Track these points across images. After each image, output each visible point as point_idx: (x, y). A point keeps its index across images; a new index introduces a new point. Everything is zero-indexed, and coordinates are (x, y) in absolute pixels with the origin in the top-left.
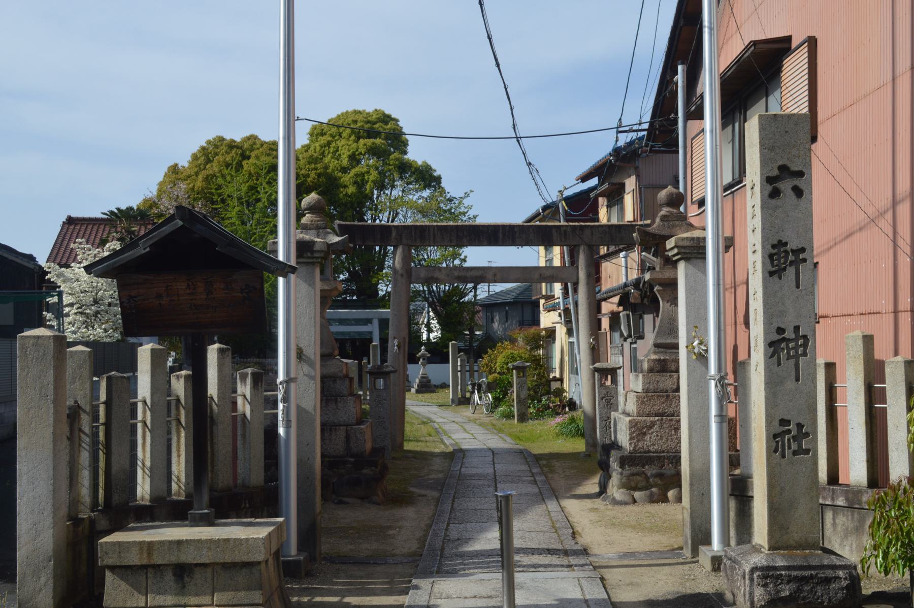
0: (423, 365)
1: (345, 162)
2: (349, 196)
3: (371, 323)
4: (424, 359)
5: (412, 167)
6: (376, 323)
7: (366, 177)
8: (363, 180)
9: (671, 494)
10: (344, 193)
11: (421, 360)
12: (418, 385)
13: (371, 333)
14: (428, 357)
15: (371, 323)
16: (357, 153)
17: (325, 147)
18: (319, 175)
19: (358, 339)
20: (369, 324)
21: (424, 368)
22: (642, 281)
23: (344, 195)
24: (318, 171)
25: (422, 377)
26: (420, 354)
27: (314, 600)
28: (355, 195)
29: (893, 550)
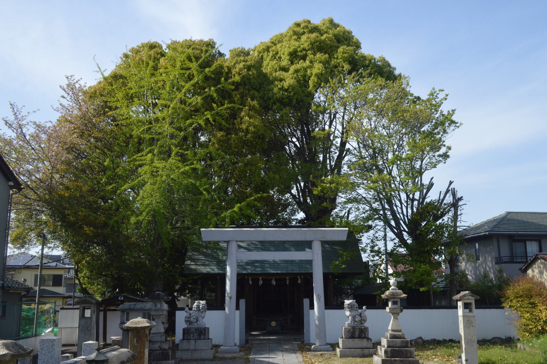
0: (395, 313)
1: (285, 62)
2: (286, 90)
3: (310, 247)
4: (394, 303)
5: (366, 59)
6: (317, 247)
7: (309, 72)
8: (304, 76)
9: (224, 245)
10: (279, 86)
11: (390, 304)
12: (386, 352)
13: (310, 262)
14: (402, 299)
15: (310, 247)
16: (299, 49)
17: (264, 52)
18: (249, 68)
19: (300, 274)
20: (307, 250)
21: (396, 318)
22: (431, 292)
23: (279, 89)
24: (248, 63)
25: (393, 337)
26: (387, 293)
27: (395, 226)
28: (293, 89)
29: (22, 178)
